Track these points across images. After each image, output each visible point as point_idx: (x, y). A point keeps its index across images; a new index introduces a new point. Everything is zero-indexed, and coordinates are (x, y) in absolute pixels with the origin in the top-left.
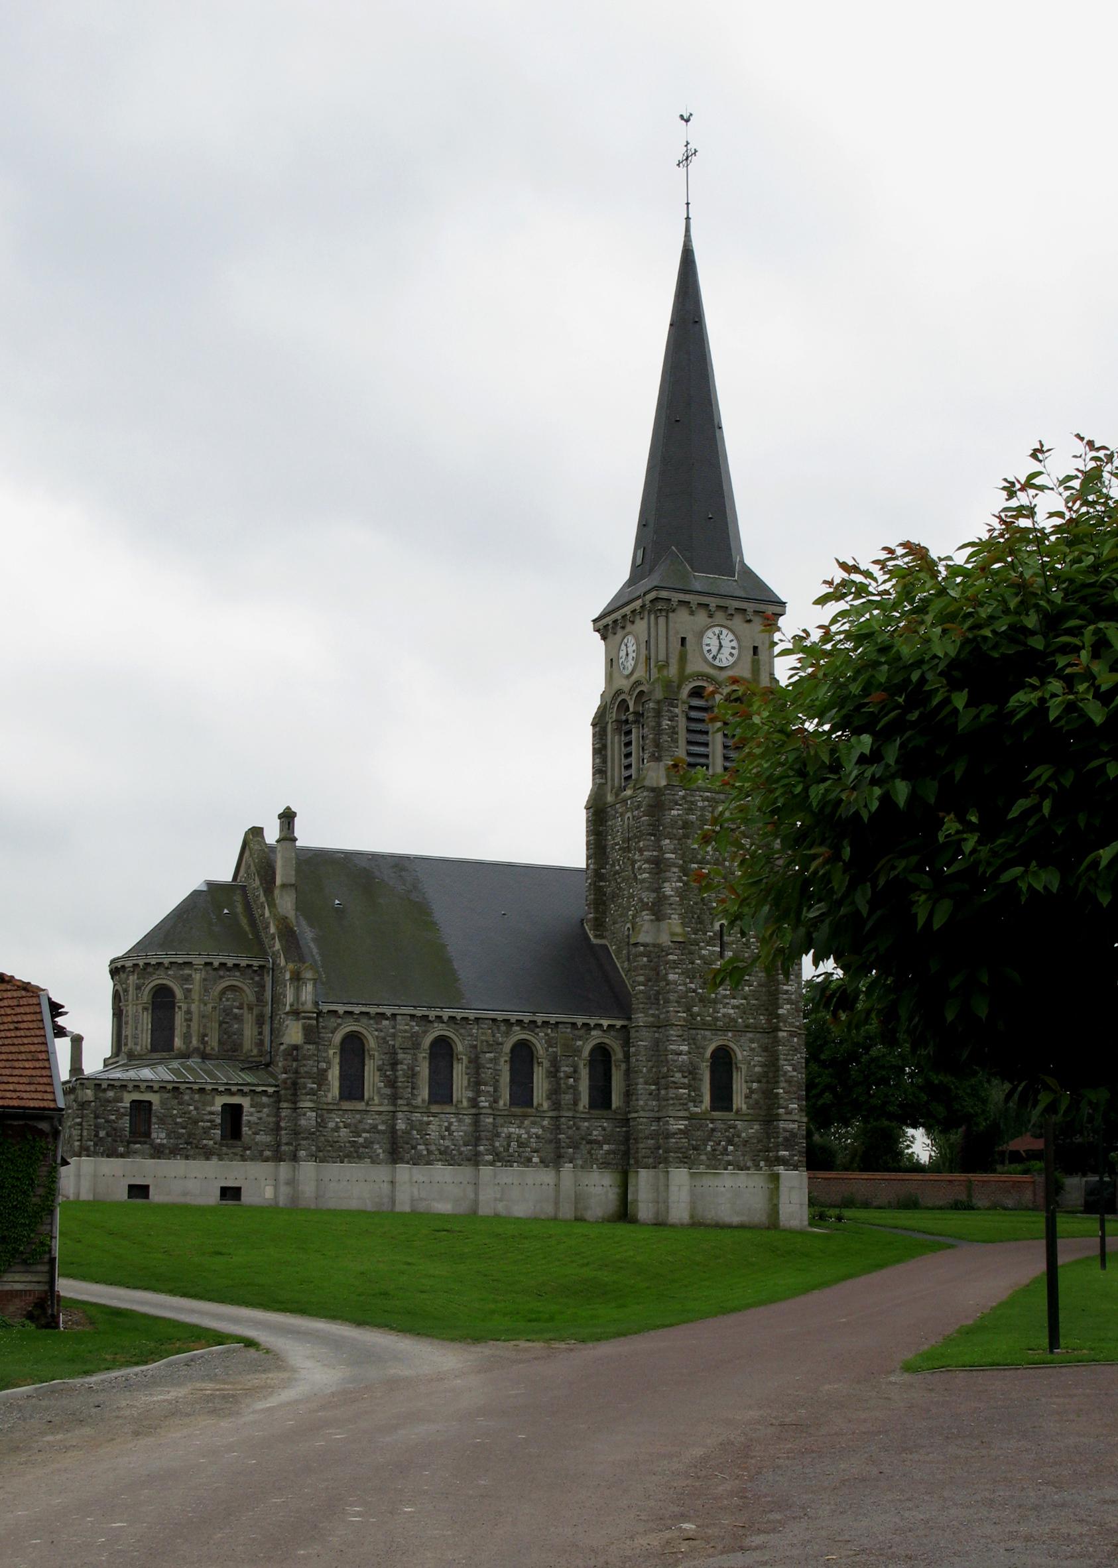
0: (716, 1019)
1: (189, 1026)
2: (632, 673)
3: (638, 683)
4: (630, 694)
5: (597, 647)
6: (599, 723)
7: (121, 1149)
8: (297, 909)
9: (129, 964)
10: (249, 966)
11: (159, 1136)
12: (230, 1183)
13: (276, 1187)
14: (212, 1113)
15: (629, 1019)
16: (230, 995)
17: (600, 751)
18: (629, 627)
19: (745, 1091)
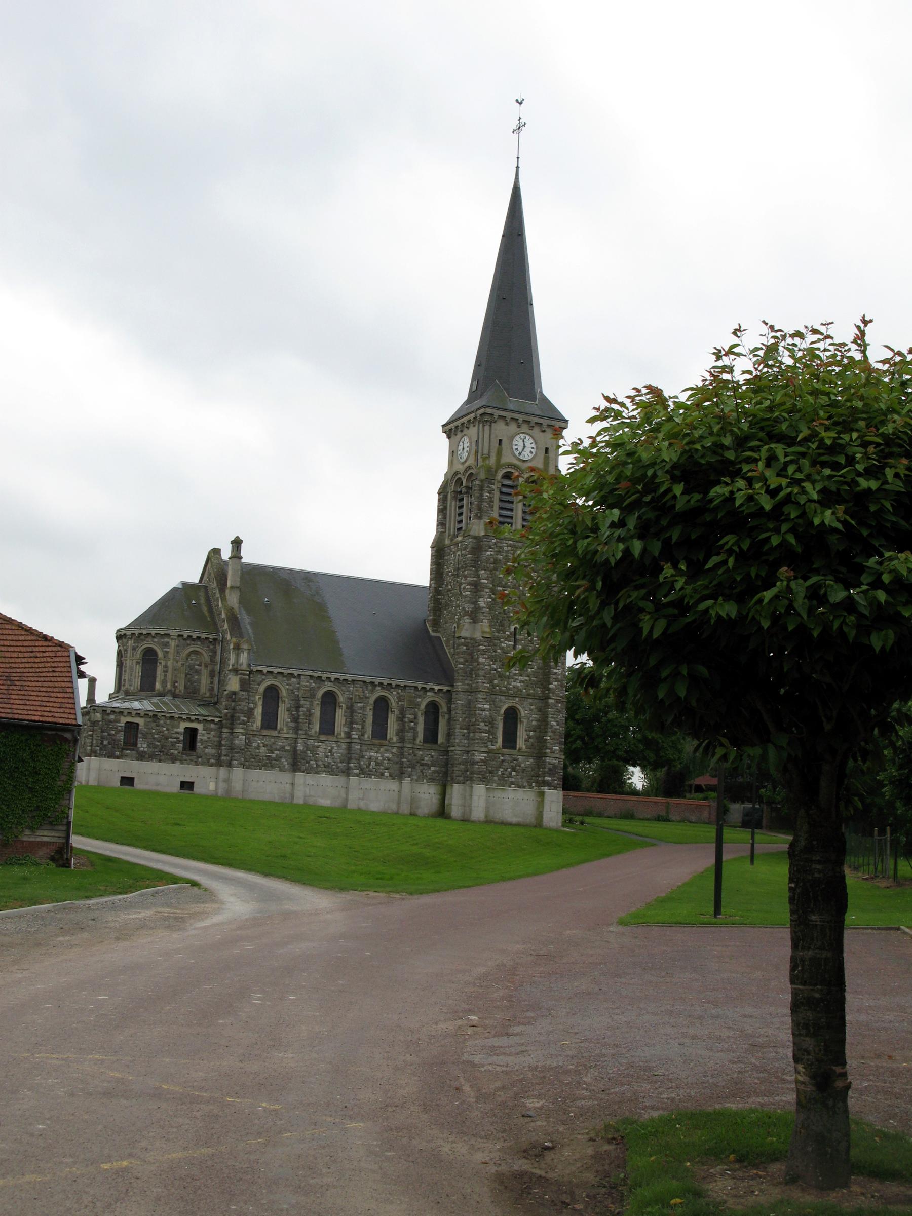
1: (165, 676)
2: (466, 461)
3: (469, 468)
5: (444, 442)
8: (240, 603)
10: (207, 638)
11: (143, 746)
13: (217, 783)
19: (525, 737)
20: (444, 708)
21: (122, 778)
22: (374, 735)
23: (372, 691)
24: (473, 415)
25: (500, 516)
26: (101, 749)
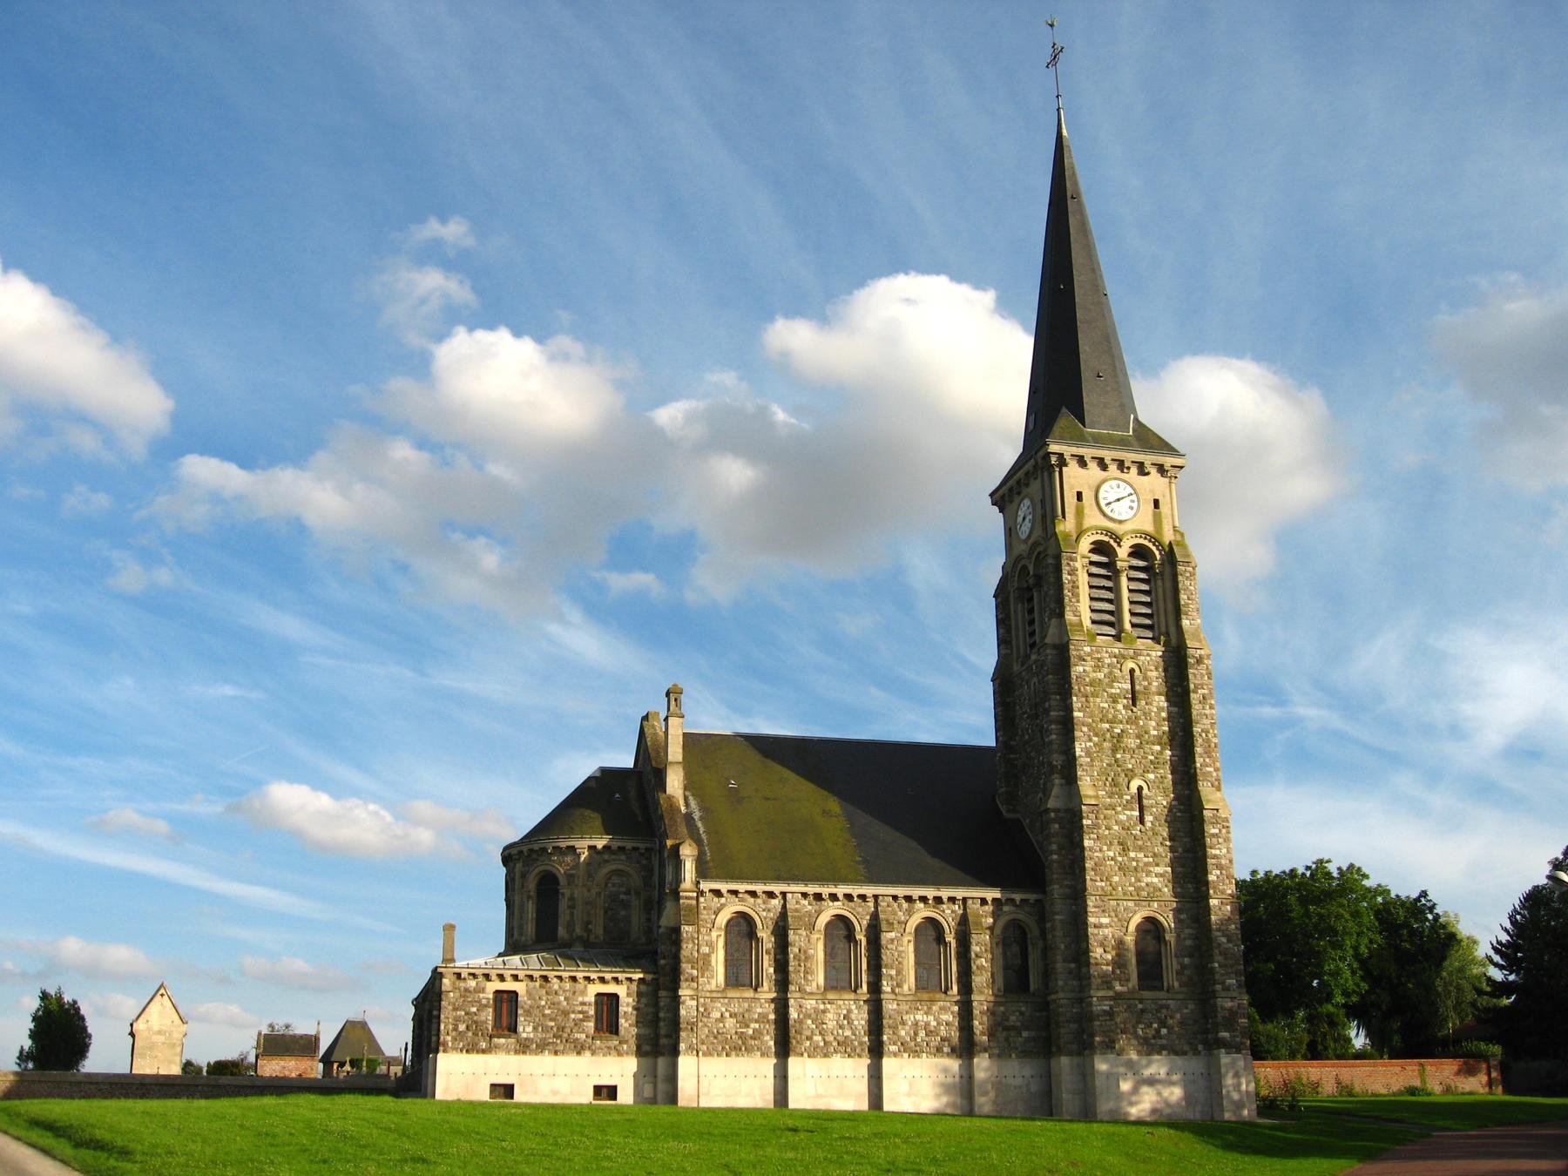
0: (1139, 889)
1: (572, 914)
2: (1029, 536)
3: (1036, 544)
4: (1029, 558)
5: (996, 518)
6: (1001, 594)
7: (484, 1045)
8: (685, 788)
9: (525, 849)
10: (635, 849)
11: (526, 1030)
12: (606, 1081)
13: (655, 1084)
14: (583, 1004)
15: (1044, 892)
16: (615, 880)
17: (1003, 622)
18: (1025, 491)
19: (1176, 966)
20: (1034, 929)
21: (493, 1086)
22: (921, 986)
23: (910, 913)
24: (1032, 462)
25: (1094, 622)
26: (454, 1039)
